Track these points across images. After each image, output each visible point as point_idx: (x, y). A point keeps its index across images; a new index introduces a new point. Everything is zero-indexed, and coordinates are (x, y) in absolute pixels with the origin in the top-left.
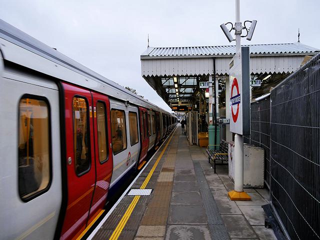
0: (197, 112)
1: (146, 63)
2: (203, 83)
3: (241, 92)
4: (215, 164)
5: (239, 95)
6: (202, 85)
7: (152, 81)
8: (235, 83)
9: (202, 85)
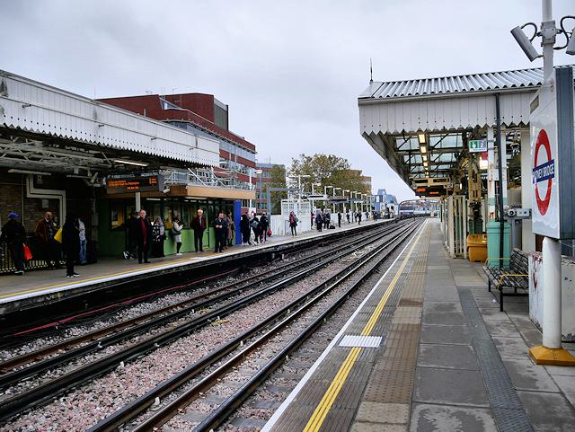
0: (464, 197)
1: (369, 111)
2: (476, 143)
3: (555, 156)
4: (502, 295)
5: (551, 162)
6: (474, 146)
7: (378, 141)
8: (543, 139)
9: (474, 146)
